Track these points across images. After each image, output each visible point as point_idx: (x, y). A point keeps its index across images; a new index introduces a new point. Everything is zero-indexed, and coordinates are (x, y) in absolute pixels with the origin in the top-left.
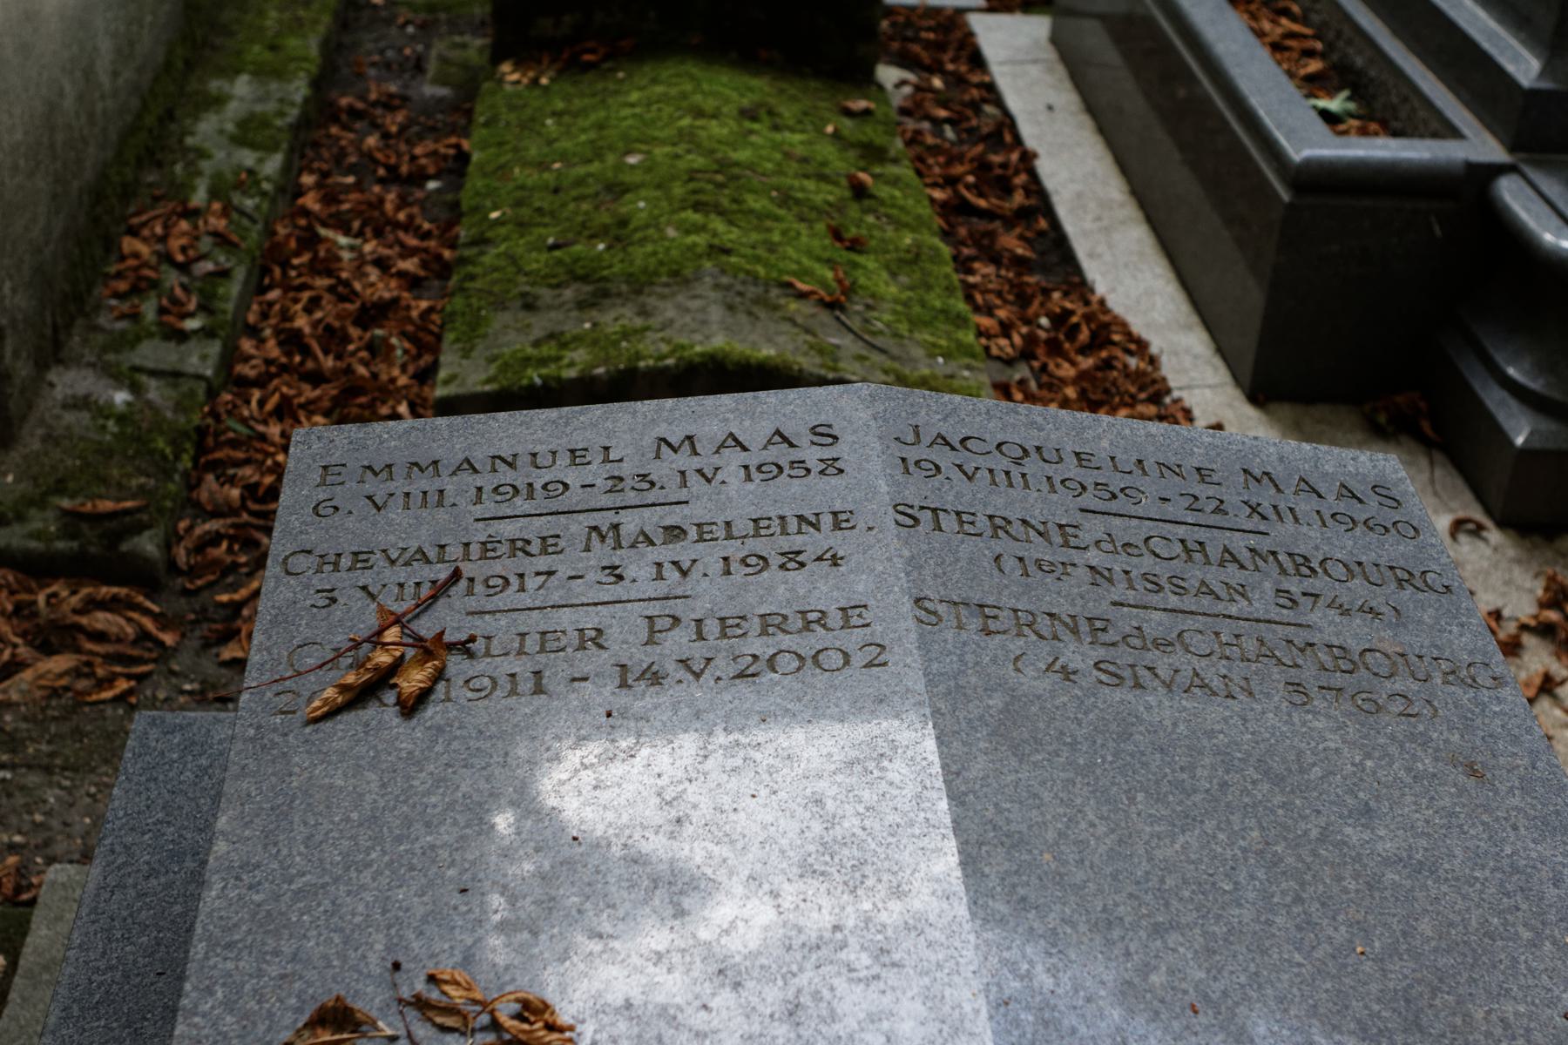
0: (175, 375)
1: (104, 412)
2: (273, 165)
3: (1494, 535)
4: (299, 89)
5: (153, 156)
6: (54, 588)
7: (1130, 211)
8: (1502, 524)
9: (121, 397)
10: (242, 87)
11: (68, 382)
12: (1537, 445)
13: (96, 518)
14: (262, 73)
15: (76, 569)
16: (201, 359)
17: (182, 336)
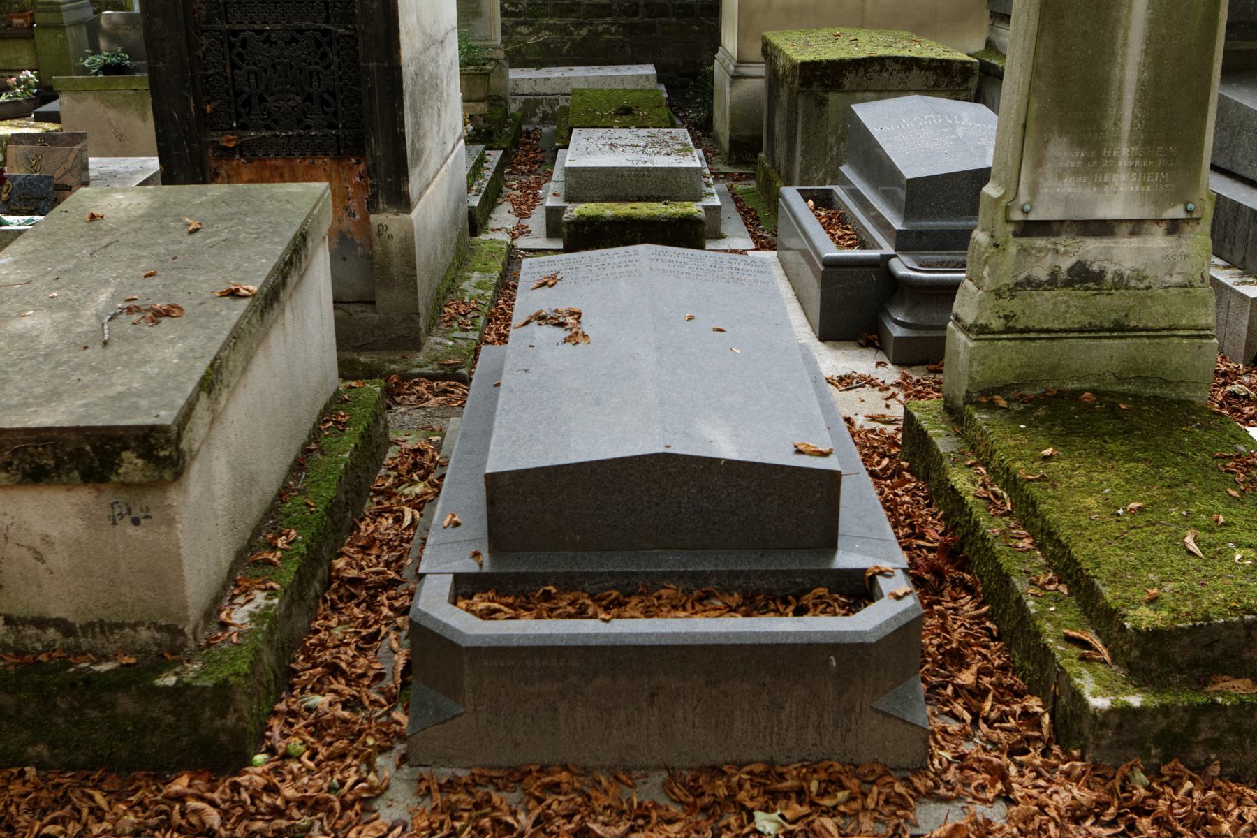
0: (466, 339)
1: (447, 346)
2: (490, 293)
3: (890, 366)
4: (496, 275)
5: (450, 290)
6: (1172, 764)
7: (795, 299)
8: (893, 364)
9: (450, 343)
10: (476, 274)
11: (433, 339)
12: (146, 129)
13: (449, 365)
14: (481, 271)
15: (444, 378)
16: (474, 335)
17: (467, 330)
